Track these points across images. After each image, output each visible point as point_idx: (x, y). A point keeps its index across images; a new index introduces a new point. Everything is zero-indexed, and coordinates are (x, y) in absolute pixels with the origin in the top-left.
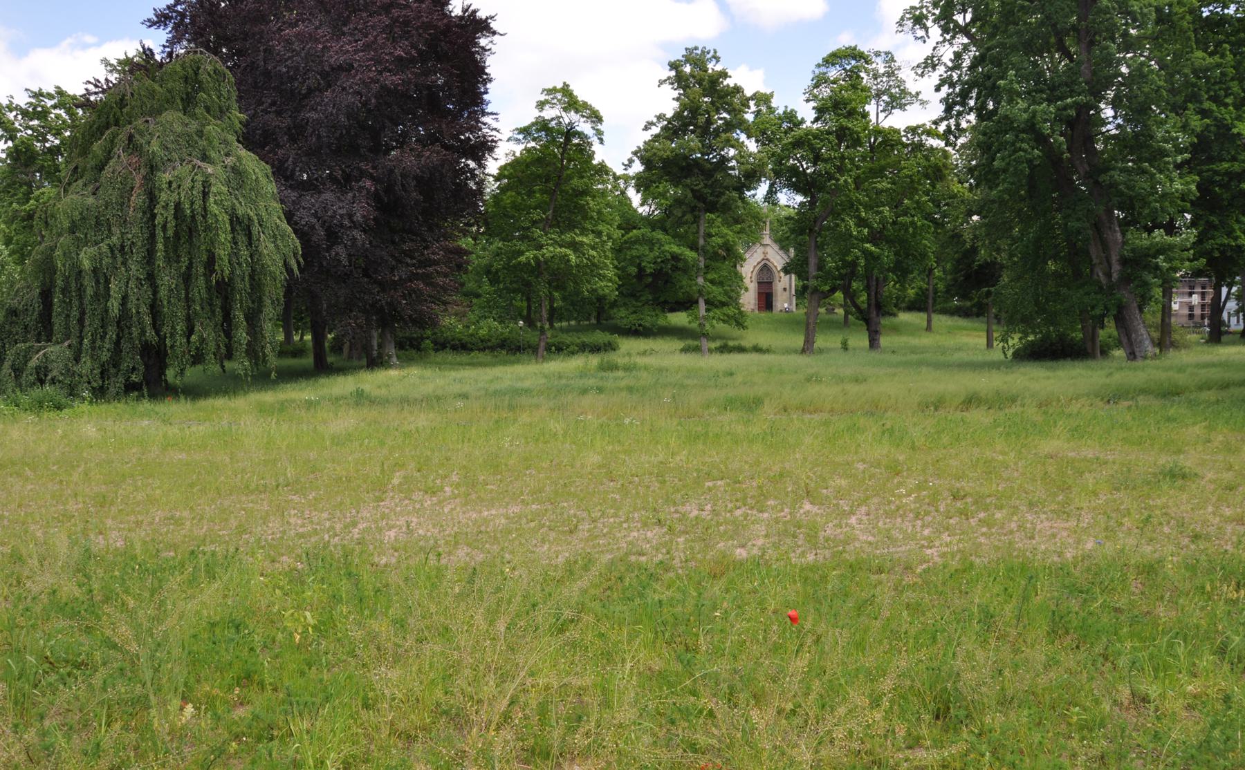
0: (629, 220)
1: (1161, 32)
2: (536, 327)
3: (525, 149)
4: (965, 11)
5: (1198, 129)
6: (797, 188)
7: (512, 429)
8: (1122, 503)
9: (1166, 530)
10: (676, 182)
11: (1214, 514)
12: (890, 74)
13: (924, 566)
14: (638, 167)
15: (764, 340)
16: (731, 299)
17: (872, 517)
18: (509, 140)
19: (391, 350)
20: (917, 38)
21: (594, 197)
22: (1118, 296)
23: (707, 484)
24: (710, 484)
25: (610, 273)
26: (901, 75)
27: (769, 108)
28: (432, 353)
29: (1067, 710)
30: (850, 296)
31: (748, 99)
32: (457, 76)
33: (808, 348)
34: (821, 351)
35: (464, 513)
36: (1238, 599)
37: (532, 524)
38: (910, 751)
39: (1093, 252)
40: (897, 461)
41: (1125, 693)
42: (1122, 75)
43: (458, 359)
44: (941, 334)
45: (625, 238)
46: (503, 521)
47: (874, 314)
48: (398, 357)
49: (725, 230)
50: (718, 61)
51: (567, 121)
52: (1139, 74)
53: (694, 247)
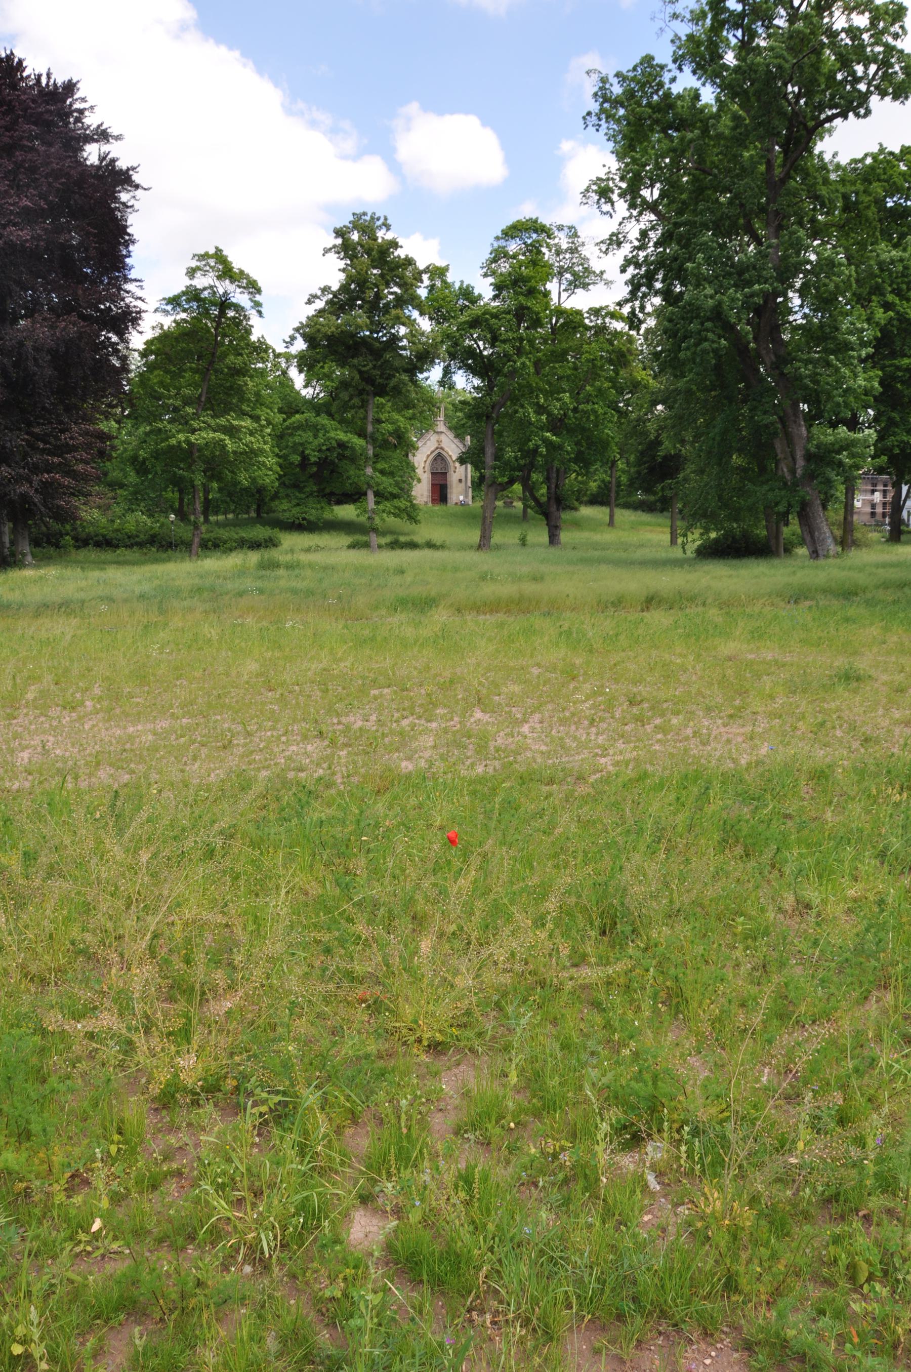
0: (291, 403)
1: (848, 220)
2: (189, 521)
3: (175, 321)
4: (652, 186)
5: (883, 322)
6: (473, 371)
7: (162, 634)
8: (798, 707)
9: (839, 733)
10: (342, 364)
11: (884, 716)
12: (573, 250)
13: (598, 775)
14: (300, 345)
15: (437, 534)
16: (403, 492)
17: (545, 725)
18: (156, 311)
19: (25, 547)
20: (602, 212)
21: (251, 377)
22: (801, 493)
23: (372, 692)
24: (376, 692)
25: (271, 461)
26: (585, 251)
27: (444, 282)
28: (73, 551)
29: (733, 920)
30: (529, 488)
31: (421, 273)
32: (95, 235)
33: (484, 544)
34: (498, 547)
35: (107, 729)
36: (900, 801)
37: (183, 740)
38: (575, 970)
39: (779, 445)
40: (573, 665)
41: (789, 901)
42: (809, 262)
43: (103, 557)
44: (624, 530)
45: (287, 423)
46: (150, 737)
47: (553, 508)
48: (34, 556)
49: (396, 416)
50: (388, 229)
51: (221, 291)
52: (827, 265)
53: (362, 434)
